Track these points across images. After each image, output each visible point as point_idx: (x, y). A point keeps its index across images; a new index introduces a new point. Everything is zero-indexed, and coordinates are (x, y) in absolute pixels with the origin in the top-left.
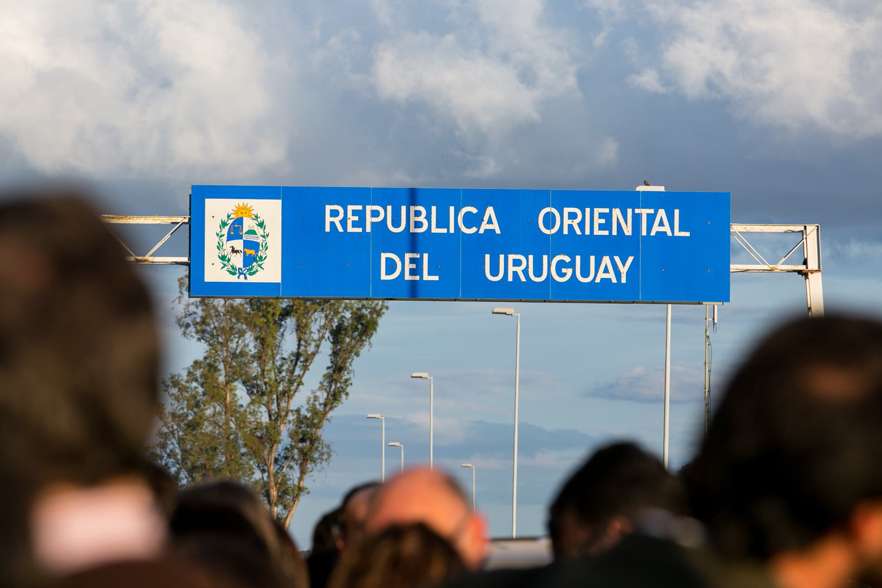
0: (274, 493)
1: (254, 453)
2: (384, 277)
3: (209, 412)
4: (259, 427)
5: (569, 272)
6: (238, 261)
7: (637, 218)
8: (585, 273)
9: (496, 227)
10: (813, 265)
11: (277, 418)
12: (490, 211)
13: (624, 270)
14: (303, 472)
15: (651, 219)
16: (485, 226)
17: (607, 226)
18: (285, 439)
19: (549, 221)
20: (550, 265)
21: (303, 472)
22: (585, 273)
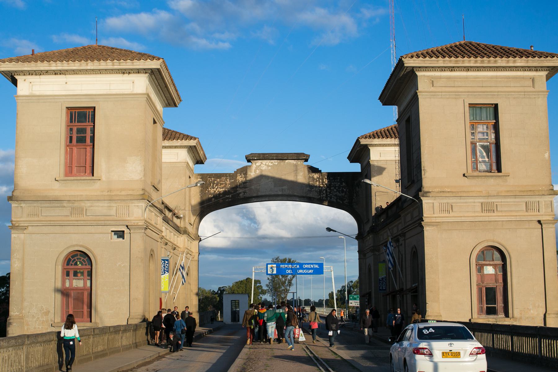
0: (285, 290)
1: (282, 285)
2: (287, 273)
3: (276, 279)
4: (283, 281)
5: (306, 272)
6: (271, 271)
7: (313, 266)
8: (308, 272)
9: (299, 267)
10: (332, 270)
11: (286, 280)
12: (298, 265)
13: (312, 271)
14: (289, 288)
15: (315, 266)
16: (297, 267)
17: (310, 267)
18: (287, 283)
19: (304, 266)
20: (304, 271)
21: (289, 288)
22: (308, 272)
